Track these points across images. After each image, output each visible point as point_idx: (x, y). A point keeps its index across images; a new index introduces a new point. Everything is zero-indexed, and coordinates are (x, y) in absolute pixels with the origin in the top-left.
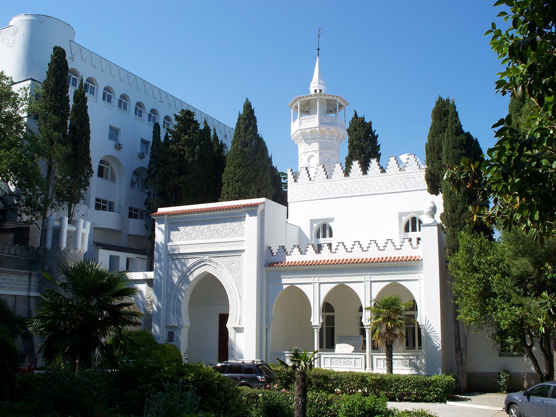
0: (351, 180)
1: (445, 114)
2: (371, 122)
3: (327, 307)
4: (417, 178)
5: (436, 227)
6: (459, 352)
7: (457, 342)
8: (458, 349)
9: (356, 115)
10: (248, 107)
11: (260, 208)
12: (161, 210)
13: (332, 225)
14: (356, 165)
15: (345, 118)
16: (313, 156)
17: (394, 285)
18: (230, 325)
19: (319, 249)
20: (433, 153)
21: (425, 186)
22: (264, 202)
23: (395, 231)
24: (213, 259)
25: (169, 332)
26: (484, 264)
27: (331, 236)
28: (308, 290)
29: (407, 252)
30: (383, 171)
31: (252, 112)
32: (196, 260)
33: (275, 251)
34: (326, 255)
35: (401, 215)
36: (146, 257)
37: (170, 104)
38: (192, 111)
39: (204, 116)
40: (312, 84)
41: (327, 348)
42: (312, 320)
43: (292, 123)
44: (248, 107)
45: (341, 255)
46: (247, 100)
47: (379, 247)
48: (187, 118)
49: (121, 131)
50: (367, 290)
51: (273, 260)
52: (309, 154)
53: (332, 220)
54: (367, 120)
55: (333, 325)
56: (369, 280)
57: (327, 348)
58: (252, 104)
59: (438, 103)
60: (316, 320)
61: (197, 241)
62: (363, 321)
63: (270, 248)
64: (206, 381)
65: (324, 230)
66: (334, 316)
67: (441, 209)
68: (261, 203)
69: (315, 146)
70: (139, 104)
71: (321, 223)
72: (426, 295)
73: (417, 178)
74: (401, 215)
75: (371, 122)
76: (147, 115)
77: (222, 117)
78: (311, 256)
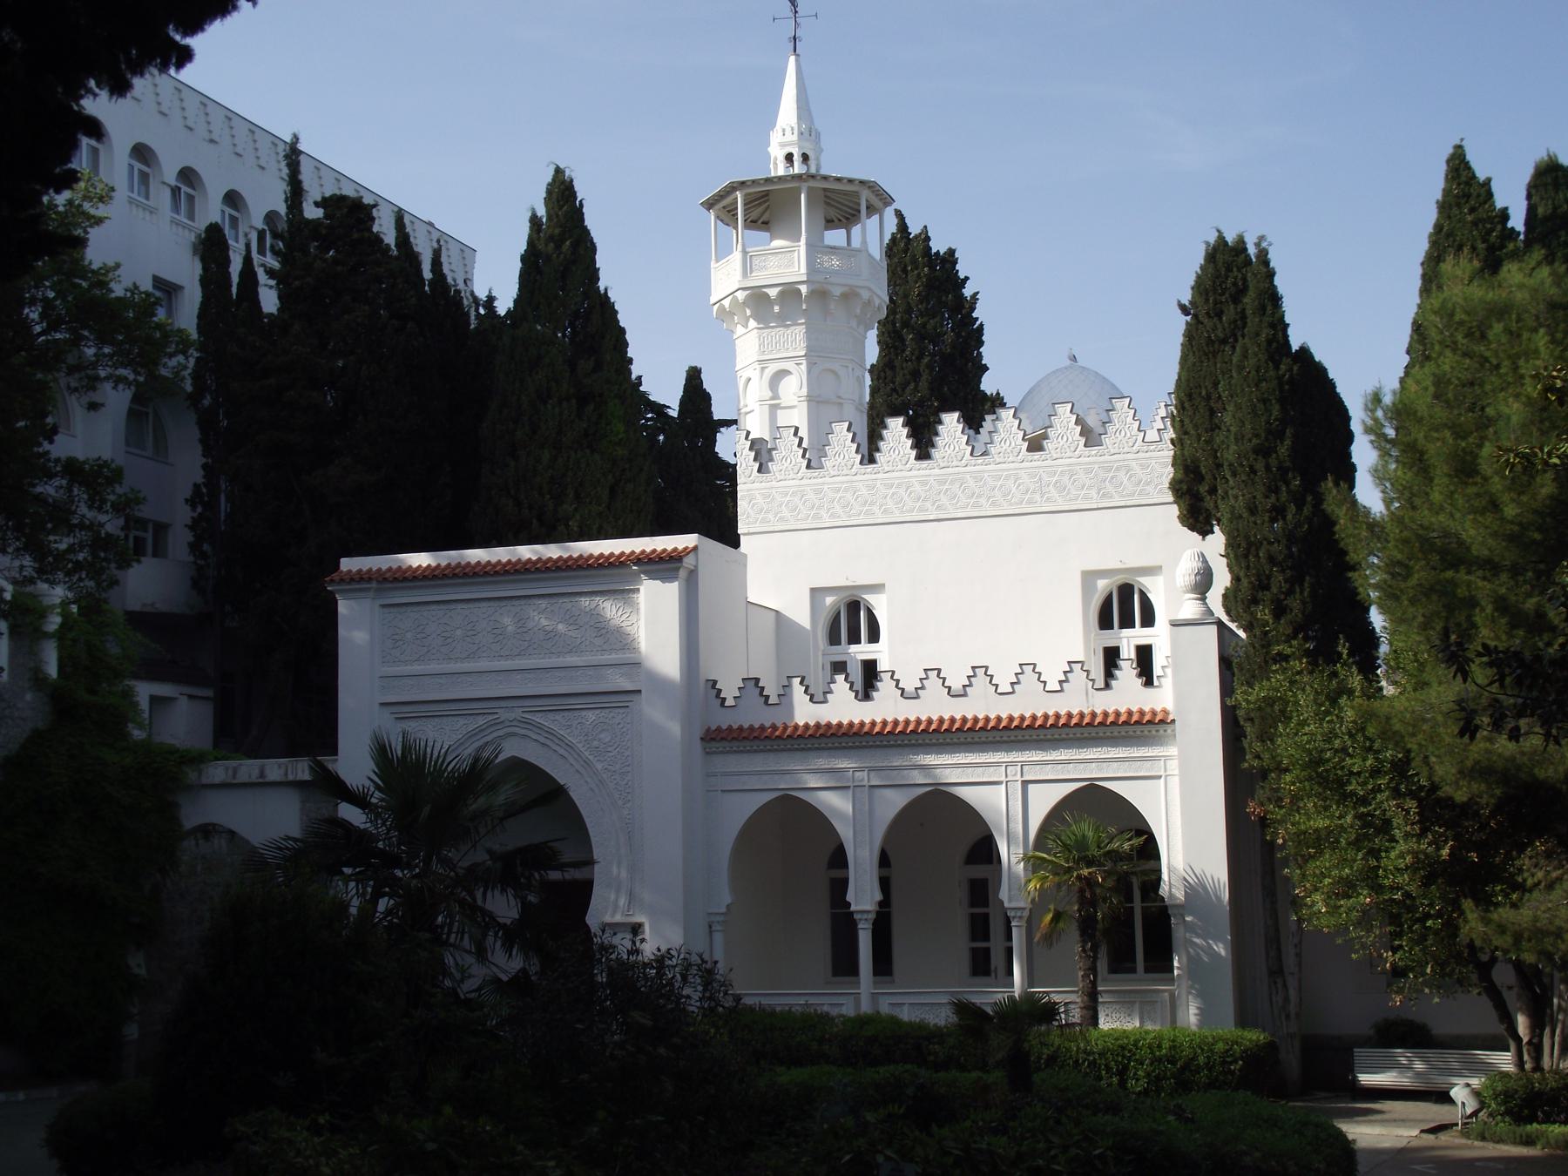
1: (1234, 296)
2: (951, 252)
3: (884, 860)
4: (1137, 469)
5: (1214, 628)
8: (1277, 972)
10: (562, 193)
11: (689, 561)
12: (348, 564)
15: (873, 235)
16: (783, 373)
20: (1195, 405)
22: (695, 548)
23: (1066, 637)
24: (538, 718)
26: (1378, 752)
27: (874, 636)
30: (1036, 445)
31: (577, 214)
32: (481, 721)
33: (730, 692)
35: (1089, 577)
36: (209, 693)
37: (164, 109)
38: (367, 200)
39: (435, 236)
40: (776, 138)
41: (1147, 970)
43: (713, 264)
44: (562, 193)
46: (559, 171)
49: (186, 291)
51: (725, 720)
52: (773, 368)
53: (877, 588)
56: (1003, 778)
57: (1147, 970)
58: (577, 186)
60: (863, 896)
61: (483, 664)
65: (852, 618)
67: (1222, 579)
69: (794, 340)
70: (188, 175)
71: (845, 597)
72: (1187, 823)
73: (1137, 469)
74: (1089, 577)
75: (951, 252)
76: (168, 193)
78: (1080, 700)
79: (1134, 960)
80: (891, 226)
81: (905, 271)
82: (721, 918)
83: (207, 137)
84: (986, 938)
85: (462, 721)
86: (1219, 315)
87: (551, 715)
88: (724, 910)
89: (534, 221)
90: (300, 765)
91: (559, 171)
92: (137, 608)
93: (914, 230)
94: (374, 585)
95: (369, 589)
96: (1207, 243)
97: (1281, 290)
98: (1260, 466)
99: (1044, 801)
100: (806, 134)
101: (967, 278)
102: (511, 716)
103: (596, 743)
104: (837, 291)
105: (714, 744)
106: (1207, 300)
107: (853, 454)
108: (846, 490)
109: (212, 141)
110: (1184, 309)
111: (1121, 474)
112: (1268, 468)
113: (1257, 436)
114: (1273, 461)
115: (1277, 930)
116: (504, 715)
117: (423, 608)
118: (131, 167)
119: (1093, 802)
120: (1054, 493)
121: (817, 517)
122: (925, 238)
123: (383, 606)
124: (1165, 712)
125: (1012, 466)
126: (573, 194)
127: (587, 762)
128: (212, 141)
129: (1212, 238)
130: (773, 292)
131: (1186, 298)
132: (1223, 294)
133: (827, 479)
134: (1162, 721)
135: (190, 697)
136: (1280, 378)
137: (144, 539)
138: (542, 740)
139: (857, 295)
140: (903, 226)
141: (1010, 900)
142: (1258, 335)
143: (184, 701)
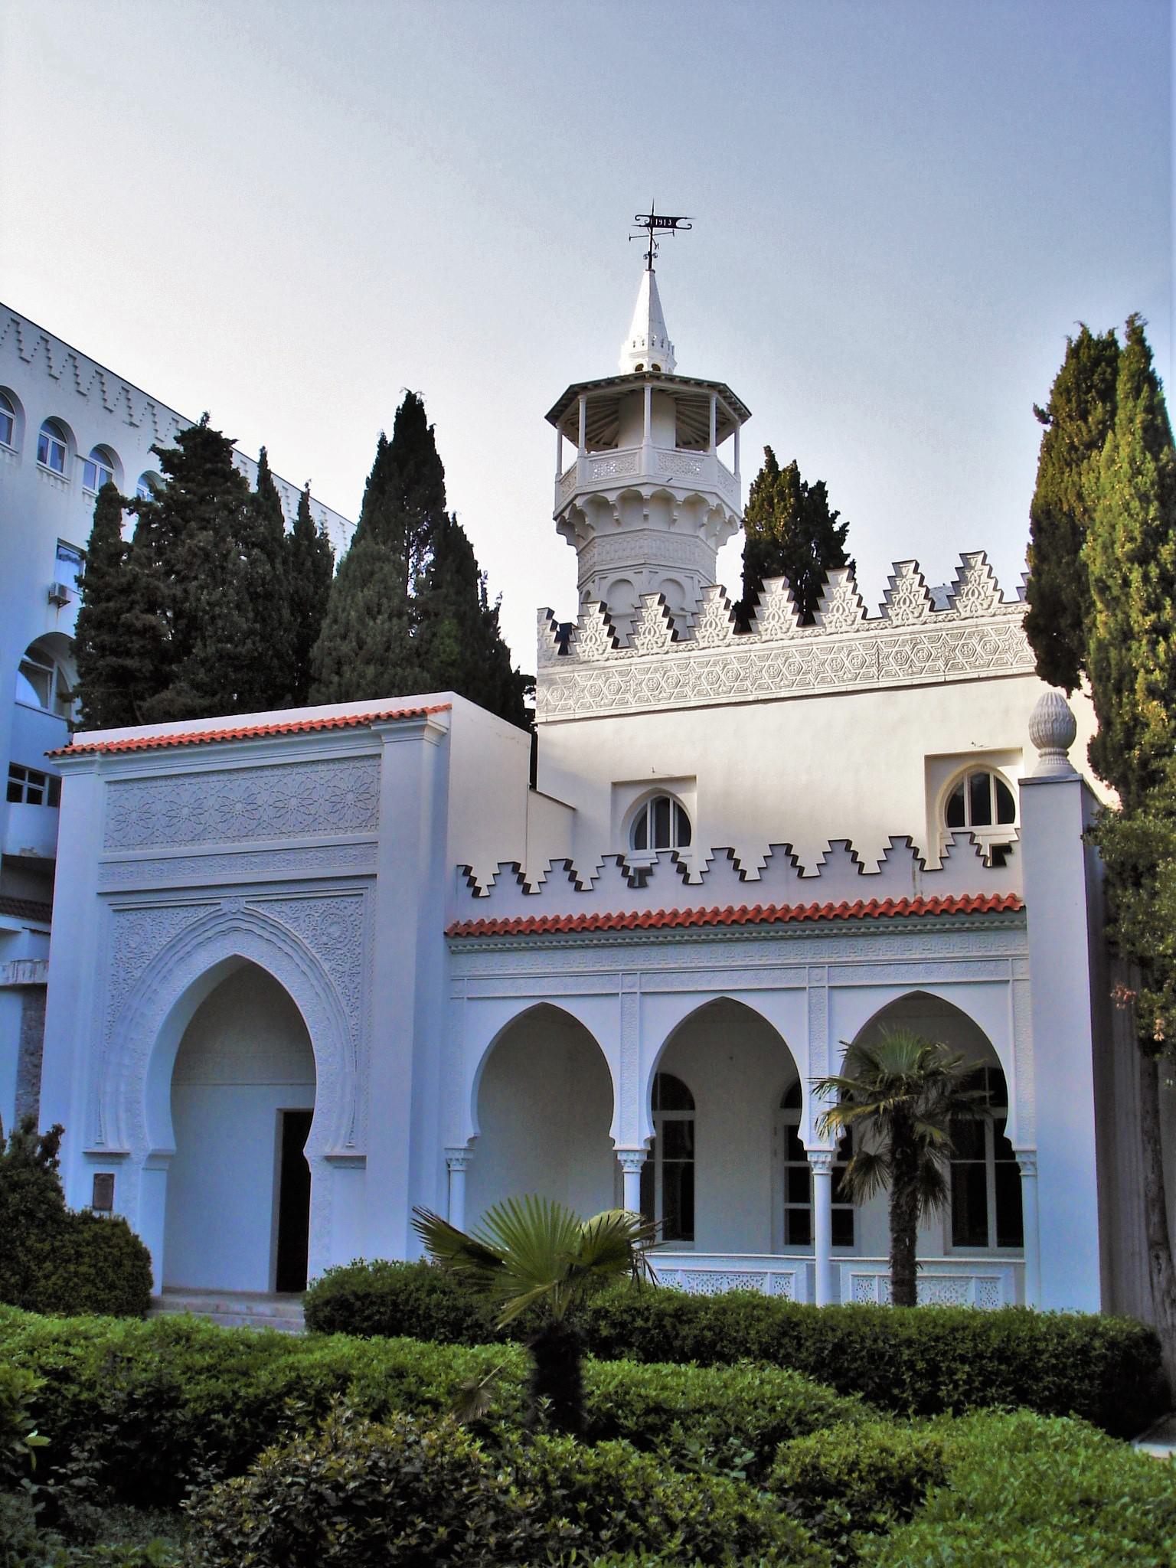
0: (758, 646)
2: (821, 485)
6: (1163, 1255)
7: (1155, 1218)
9: (771, 462)
10: (411, 414)
11: (436, 720)
13: (691, 801)
14: (777, 593)
17: (919, 1010)
18: (313, 1150)
19: (639, 879)
21: (1027, 657)
24: (262, 909)
25: (96, 1176)
28: (599, 1021)
29: (970, 881)
32: (202, 913)
34: (664, 896)
35: (934, 763)
41: (1000, 1244)
42: (613, 1133)
44: (411, 414)
45: (724, 895)
46: (411, 398)
47: (862, 865)
48: (202, 453)
50: (819, 1022)
51: (476, 913)
53: (688, 780)
54: (809, 477)
55: (691, 1155)
57: (1000, 1244)
58: (427, 410)
59: (1074, 353)
62: (802, 1135)
63: (467, 870)
64: (645, 1331)
66: (691, 1124)
68: (435, 710)
74: (934, 763)
75: (821, 485)
77: (329, 479)
78: (615, 899)
79: (985, 1234)
80: (761, 462)
81: (771, 505)
82: (461, 1155)
83: (127, 419)
84: (835, 1214)
85: (182, 913)
86: (1084, 416)
87: (277, 906)
88: (464, 1145)
89: (383, 440)
90: (927, 1302)
91: (411, 398)
92: (16, 852)
93: (783, 464)
94: (98, 757)
95: (92, 763)
96: (1070, 340)
97: (1158, 374)
98: (1136, 576)
99: (856, 1013)
100: (658, 344)
101: (837, 513)
102: (234, 907)
103: (325, 939)
104: (680, 496)
105: (459, 941)
106: (1069, 401)
107: (660, 617)
108: (656, 670)
109: (132, 424)
110: (1042, 416)
111: (974, 641)
112: (1146, 579)
113: (1132, 539)
114: (1154, 571)
115: (1161, 1188)
116: (226, 906)
117: (149, 784)
118: (43, 441)
119: (919, 1010)
120: (894, 667)
121: (623, 702)
122: (794, 471)
123: (109, 783)
124: (1013, 897)
125: (845, 636)
126: (423, 418)
127: (313, 961)
128: (132, 424)
129: (1076, 334)
130: (612, 497)
131: (1044, 401)
132: (1088, 391)
133: (636, 660)
134: (1008, 908)
135: (33, 931)
136: (1160, 471)
137: (40, 793)
138: (266, 935)
139: (703, 501)
140: (771, 462)
141: (811, 1141)
142: (1131, 420)
143: (26, 934)
